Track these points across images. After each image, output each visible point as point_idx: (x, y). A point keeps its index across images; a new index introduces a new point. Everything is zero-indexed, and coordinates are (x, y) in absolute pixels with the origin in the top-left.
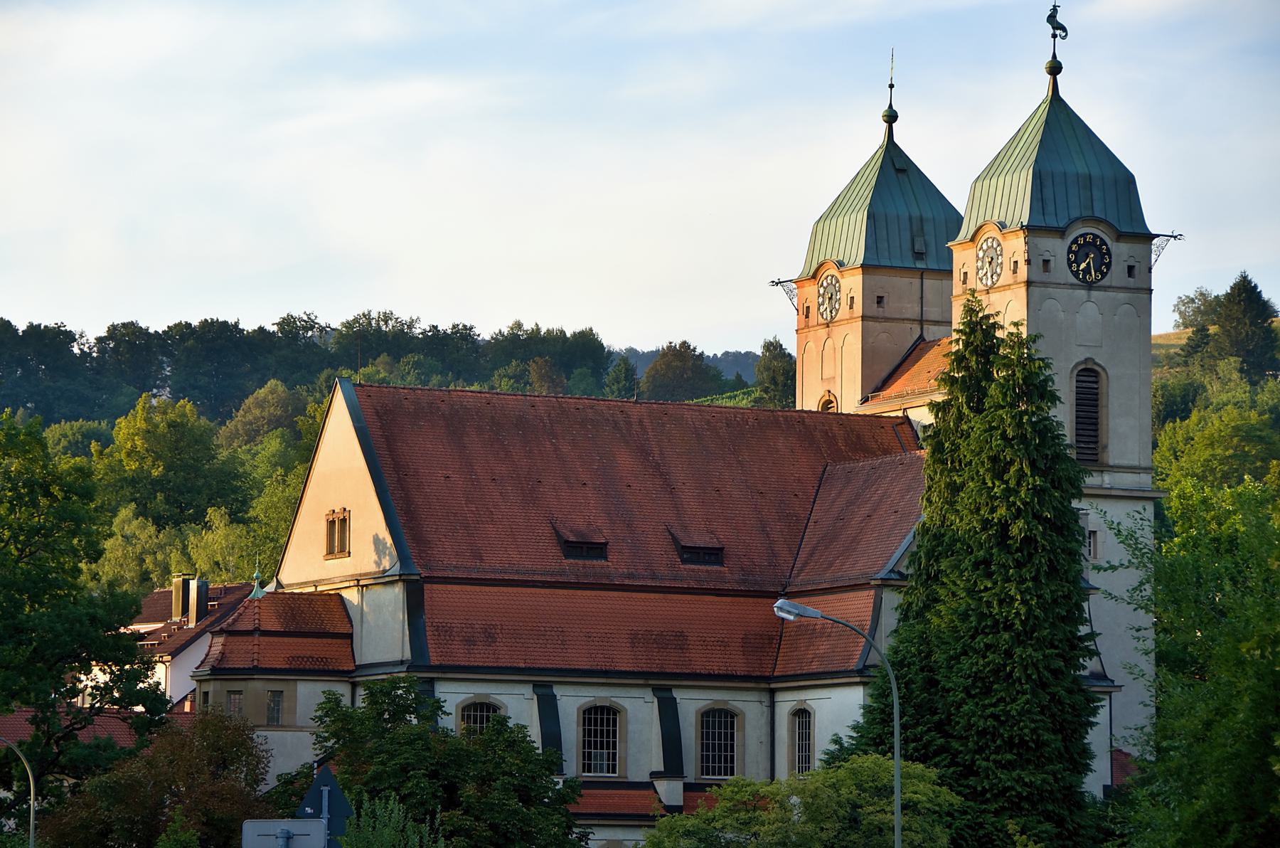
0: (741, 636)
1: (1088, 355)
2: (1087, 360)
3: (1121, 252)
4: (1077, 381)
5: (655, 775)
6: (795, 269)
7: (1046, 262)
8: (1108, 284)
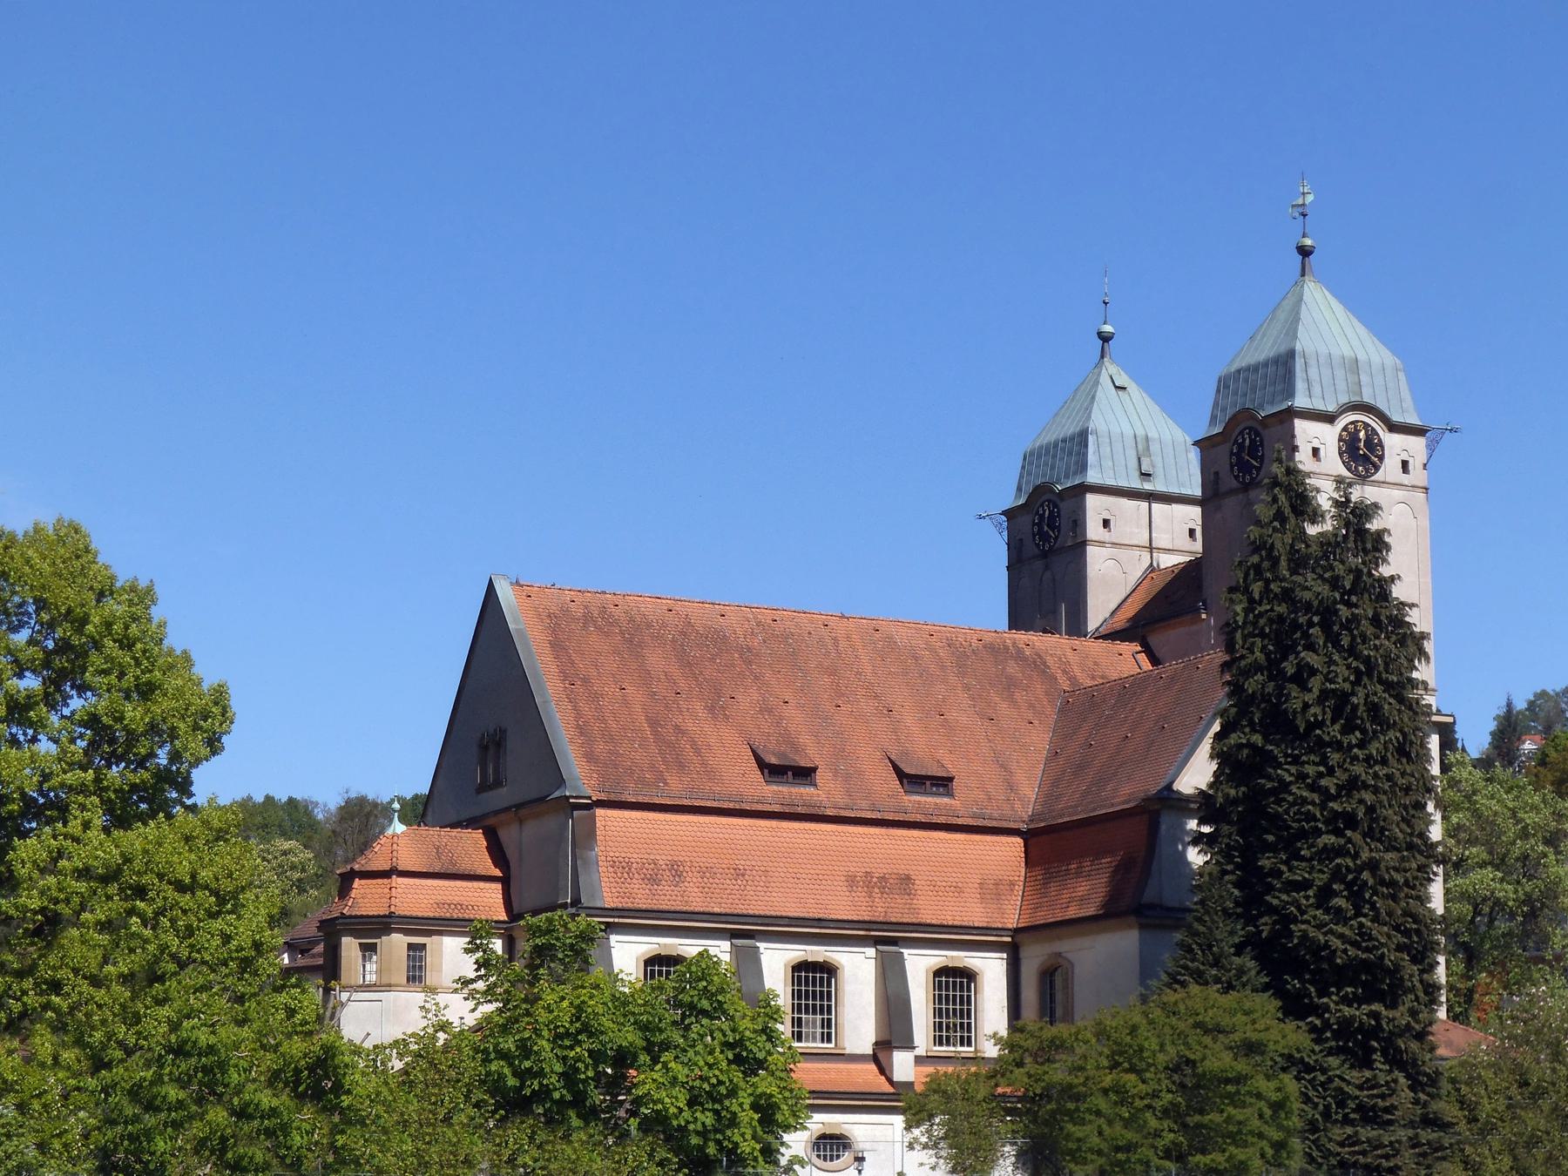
0: (979, 881)
8: (1382, 479)
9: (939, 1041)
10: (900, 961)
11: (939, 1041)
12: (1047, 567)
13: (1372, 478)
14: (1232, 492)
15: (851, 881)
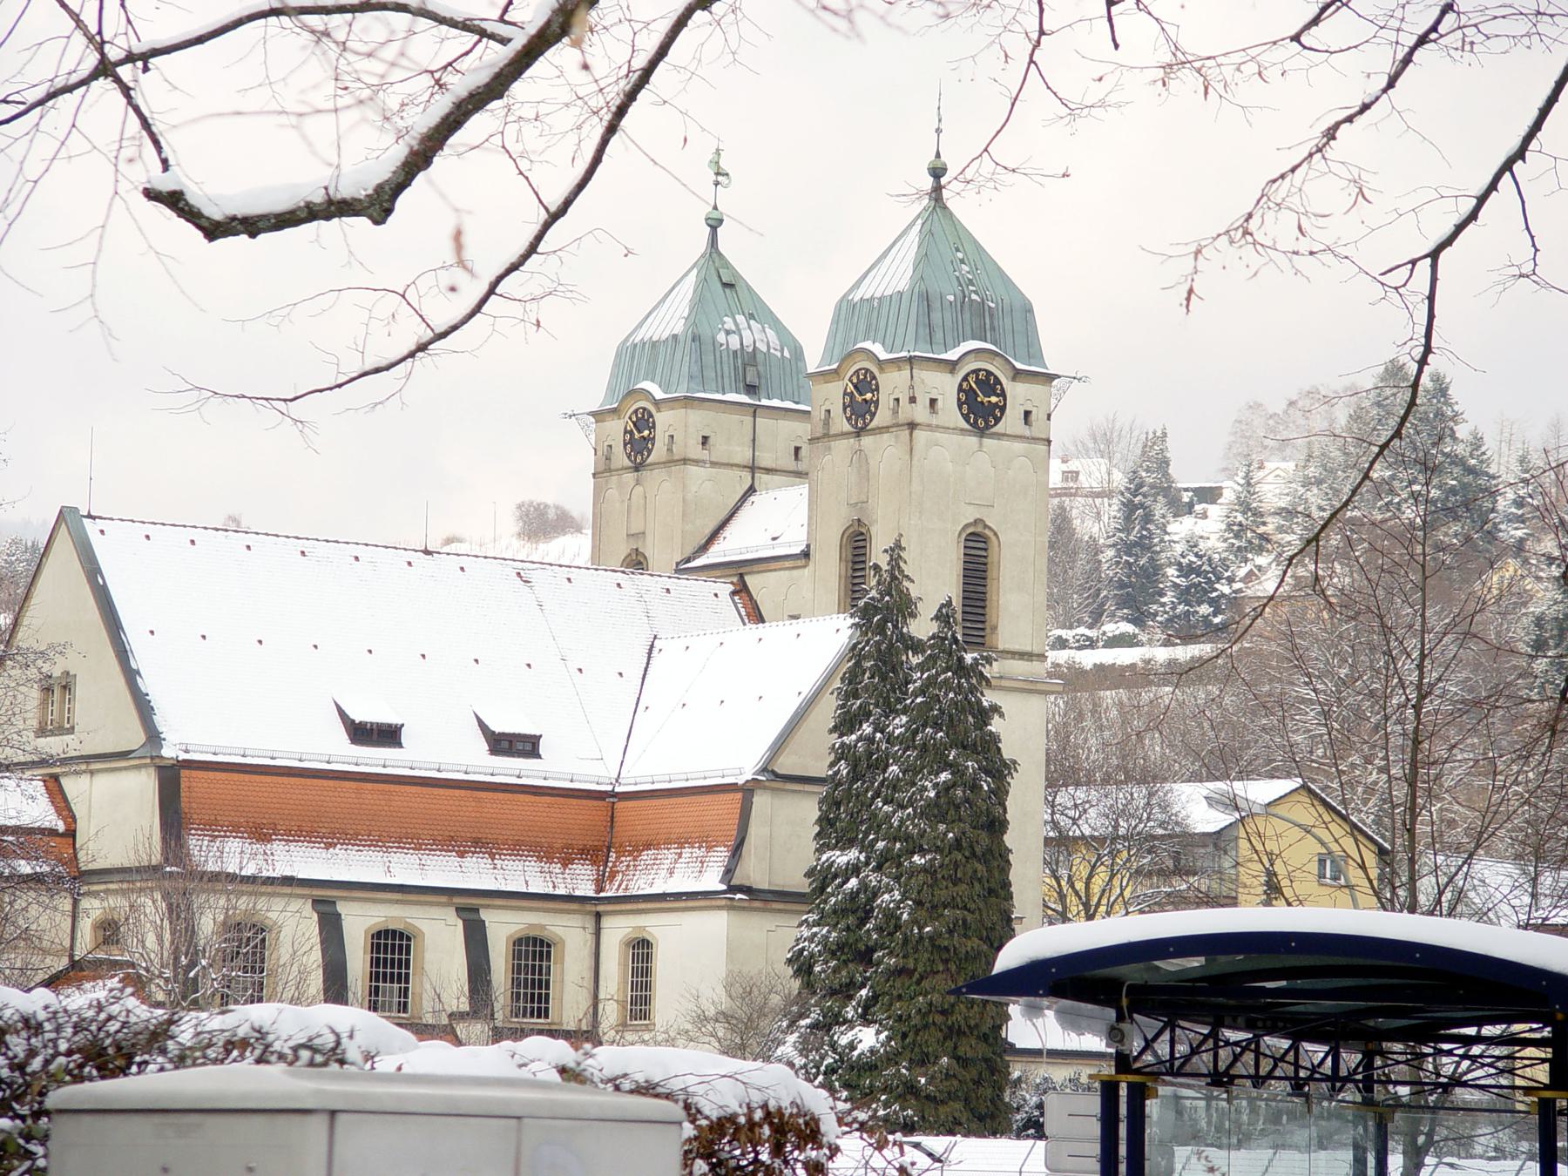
2: (976, 522)
4: (965, 547)
6: (596, 401)
7: (933, 402)
12: (638, 483)
13: (993, 430)
14: (844, 435)
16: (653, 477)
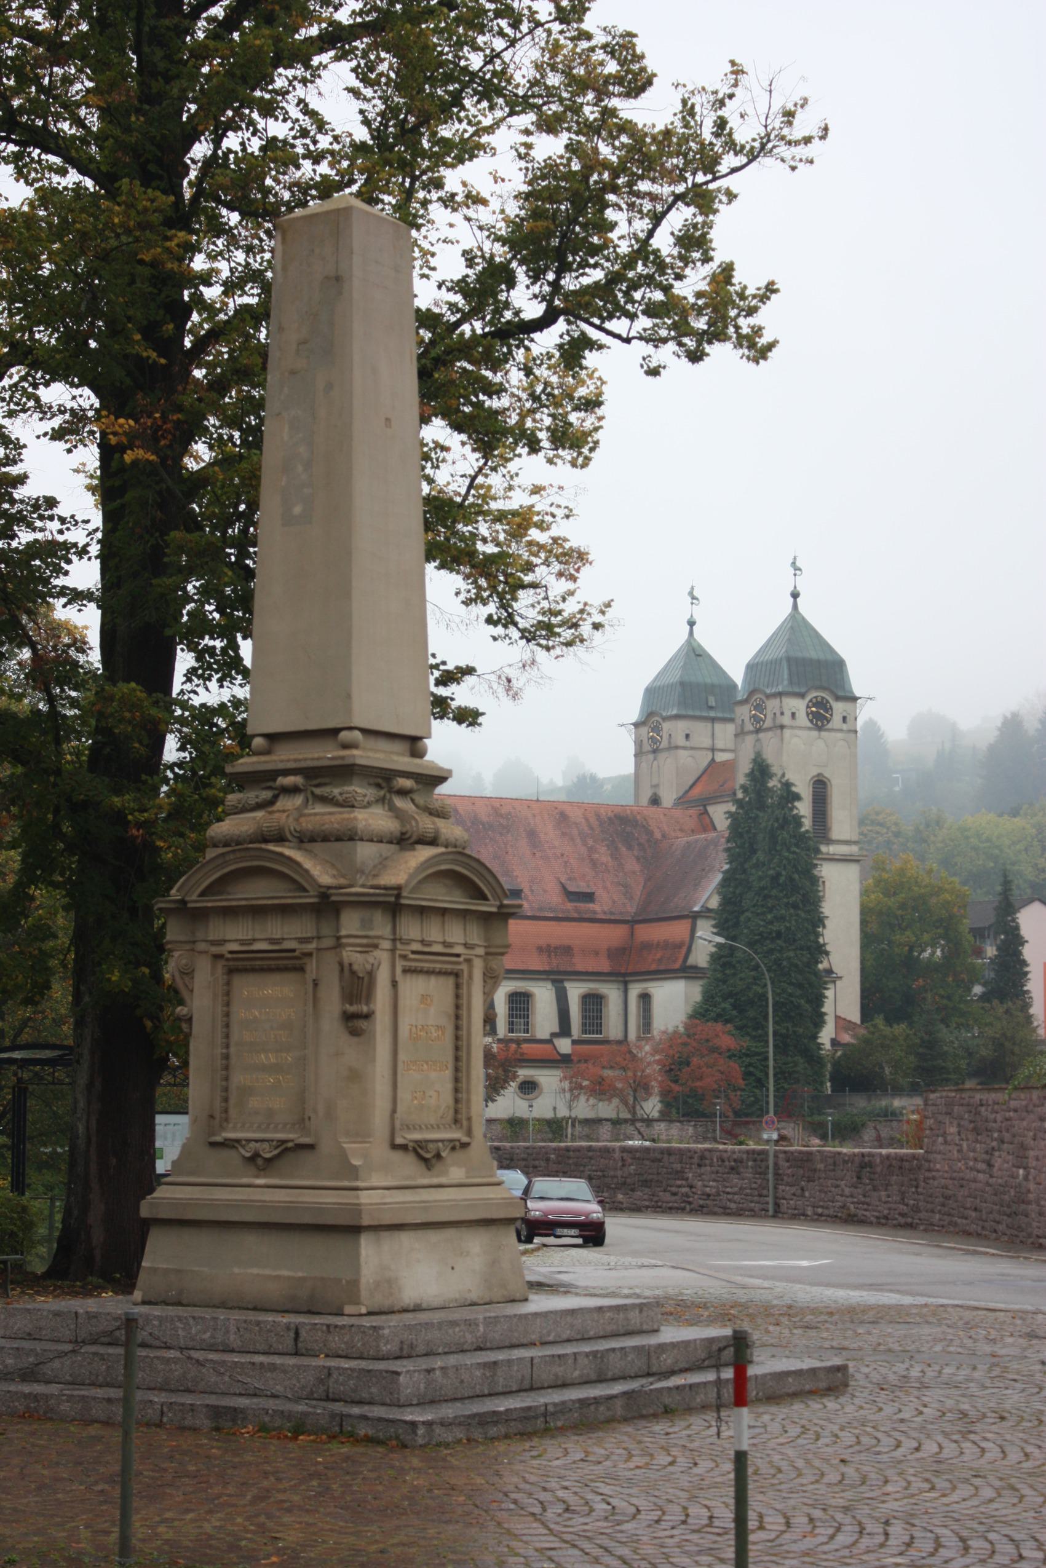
1: (819, 771)
2: (819, 775)
3: (839, 708)
5: (554, 1035)
9: (585, 1032)
10: (565, 990)
11: (585, 1032)
15: (540, 949)
16: (662, 756)
